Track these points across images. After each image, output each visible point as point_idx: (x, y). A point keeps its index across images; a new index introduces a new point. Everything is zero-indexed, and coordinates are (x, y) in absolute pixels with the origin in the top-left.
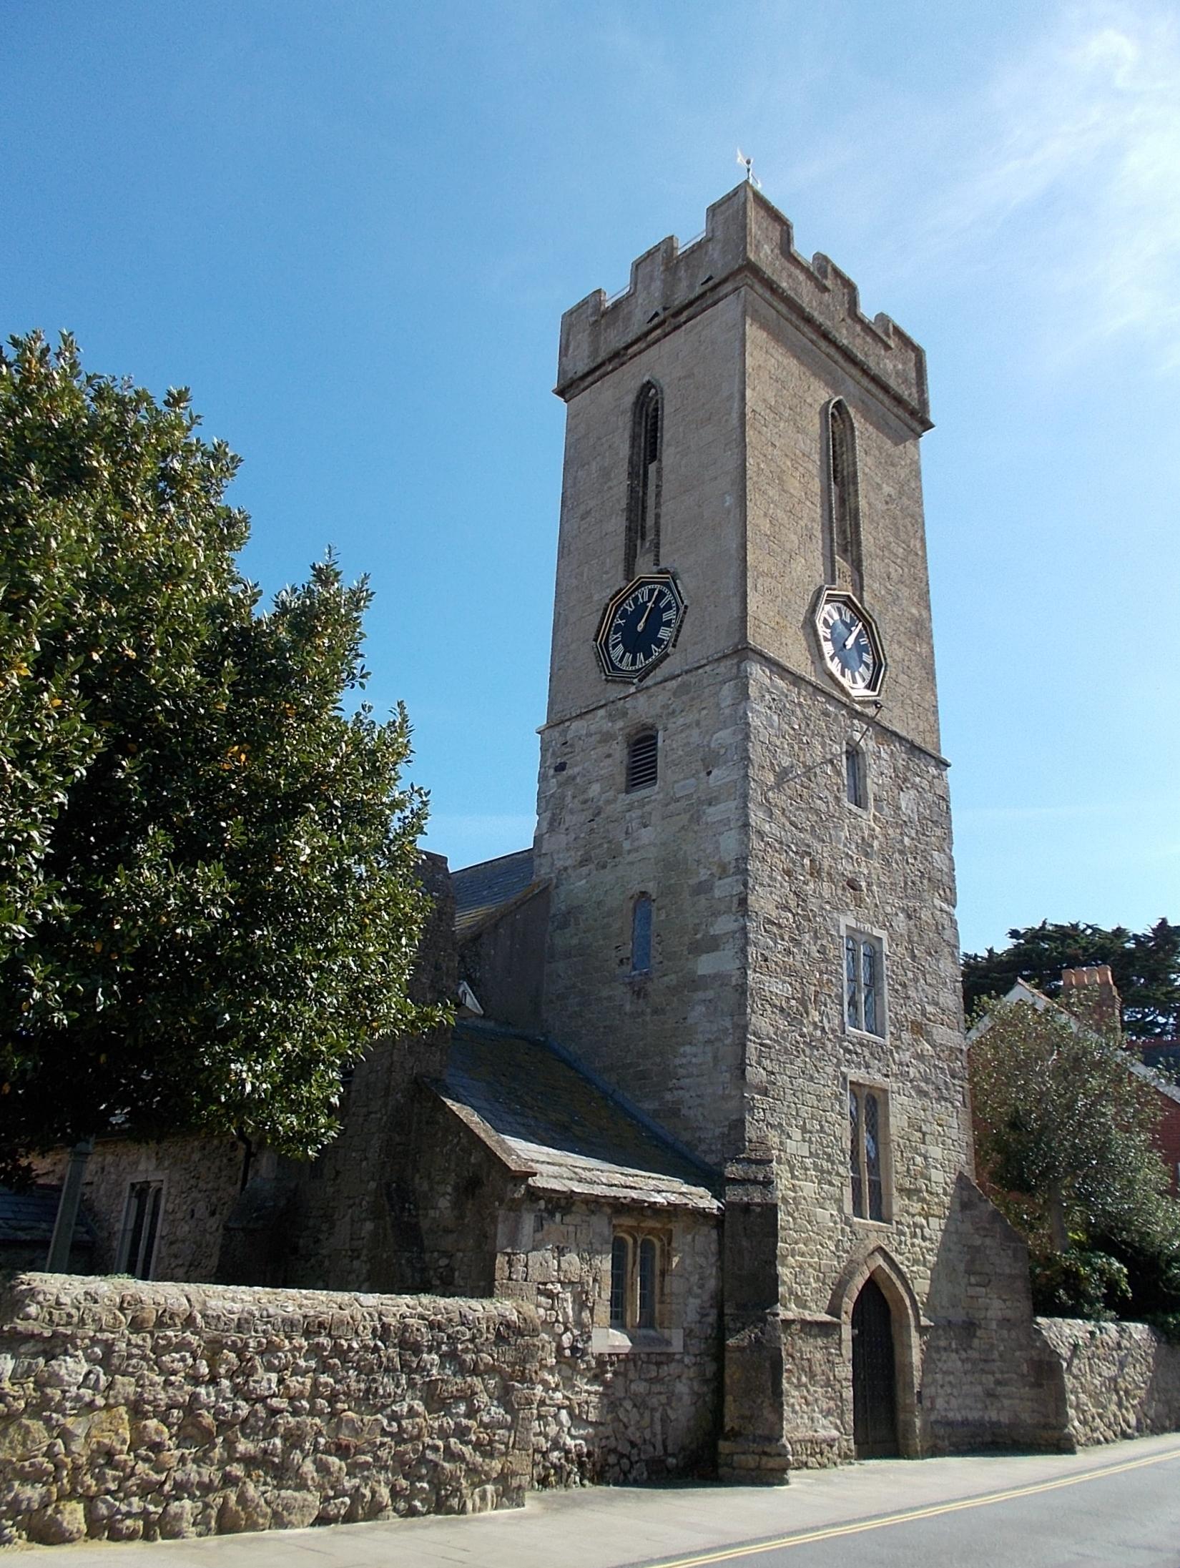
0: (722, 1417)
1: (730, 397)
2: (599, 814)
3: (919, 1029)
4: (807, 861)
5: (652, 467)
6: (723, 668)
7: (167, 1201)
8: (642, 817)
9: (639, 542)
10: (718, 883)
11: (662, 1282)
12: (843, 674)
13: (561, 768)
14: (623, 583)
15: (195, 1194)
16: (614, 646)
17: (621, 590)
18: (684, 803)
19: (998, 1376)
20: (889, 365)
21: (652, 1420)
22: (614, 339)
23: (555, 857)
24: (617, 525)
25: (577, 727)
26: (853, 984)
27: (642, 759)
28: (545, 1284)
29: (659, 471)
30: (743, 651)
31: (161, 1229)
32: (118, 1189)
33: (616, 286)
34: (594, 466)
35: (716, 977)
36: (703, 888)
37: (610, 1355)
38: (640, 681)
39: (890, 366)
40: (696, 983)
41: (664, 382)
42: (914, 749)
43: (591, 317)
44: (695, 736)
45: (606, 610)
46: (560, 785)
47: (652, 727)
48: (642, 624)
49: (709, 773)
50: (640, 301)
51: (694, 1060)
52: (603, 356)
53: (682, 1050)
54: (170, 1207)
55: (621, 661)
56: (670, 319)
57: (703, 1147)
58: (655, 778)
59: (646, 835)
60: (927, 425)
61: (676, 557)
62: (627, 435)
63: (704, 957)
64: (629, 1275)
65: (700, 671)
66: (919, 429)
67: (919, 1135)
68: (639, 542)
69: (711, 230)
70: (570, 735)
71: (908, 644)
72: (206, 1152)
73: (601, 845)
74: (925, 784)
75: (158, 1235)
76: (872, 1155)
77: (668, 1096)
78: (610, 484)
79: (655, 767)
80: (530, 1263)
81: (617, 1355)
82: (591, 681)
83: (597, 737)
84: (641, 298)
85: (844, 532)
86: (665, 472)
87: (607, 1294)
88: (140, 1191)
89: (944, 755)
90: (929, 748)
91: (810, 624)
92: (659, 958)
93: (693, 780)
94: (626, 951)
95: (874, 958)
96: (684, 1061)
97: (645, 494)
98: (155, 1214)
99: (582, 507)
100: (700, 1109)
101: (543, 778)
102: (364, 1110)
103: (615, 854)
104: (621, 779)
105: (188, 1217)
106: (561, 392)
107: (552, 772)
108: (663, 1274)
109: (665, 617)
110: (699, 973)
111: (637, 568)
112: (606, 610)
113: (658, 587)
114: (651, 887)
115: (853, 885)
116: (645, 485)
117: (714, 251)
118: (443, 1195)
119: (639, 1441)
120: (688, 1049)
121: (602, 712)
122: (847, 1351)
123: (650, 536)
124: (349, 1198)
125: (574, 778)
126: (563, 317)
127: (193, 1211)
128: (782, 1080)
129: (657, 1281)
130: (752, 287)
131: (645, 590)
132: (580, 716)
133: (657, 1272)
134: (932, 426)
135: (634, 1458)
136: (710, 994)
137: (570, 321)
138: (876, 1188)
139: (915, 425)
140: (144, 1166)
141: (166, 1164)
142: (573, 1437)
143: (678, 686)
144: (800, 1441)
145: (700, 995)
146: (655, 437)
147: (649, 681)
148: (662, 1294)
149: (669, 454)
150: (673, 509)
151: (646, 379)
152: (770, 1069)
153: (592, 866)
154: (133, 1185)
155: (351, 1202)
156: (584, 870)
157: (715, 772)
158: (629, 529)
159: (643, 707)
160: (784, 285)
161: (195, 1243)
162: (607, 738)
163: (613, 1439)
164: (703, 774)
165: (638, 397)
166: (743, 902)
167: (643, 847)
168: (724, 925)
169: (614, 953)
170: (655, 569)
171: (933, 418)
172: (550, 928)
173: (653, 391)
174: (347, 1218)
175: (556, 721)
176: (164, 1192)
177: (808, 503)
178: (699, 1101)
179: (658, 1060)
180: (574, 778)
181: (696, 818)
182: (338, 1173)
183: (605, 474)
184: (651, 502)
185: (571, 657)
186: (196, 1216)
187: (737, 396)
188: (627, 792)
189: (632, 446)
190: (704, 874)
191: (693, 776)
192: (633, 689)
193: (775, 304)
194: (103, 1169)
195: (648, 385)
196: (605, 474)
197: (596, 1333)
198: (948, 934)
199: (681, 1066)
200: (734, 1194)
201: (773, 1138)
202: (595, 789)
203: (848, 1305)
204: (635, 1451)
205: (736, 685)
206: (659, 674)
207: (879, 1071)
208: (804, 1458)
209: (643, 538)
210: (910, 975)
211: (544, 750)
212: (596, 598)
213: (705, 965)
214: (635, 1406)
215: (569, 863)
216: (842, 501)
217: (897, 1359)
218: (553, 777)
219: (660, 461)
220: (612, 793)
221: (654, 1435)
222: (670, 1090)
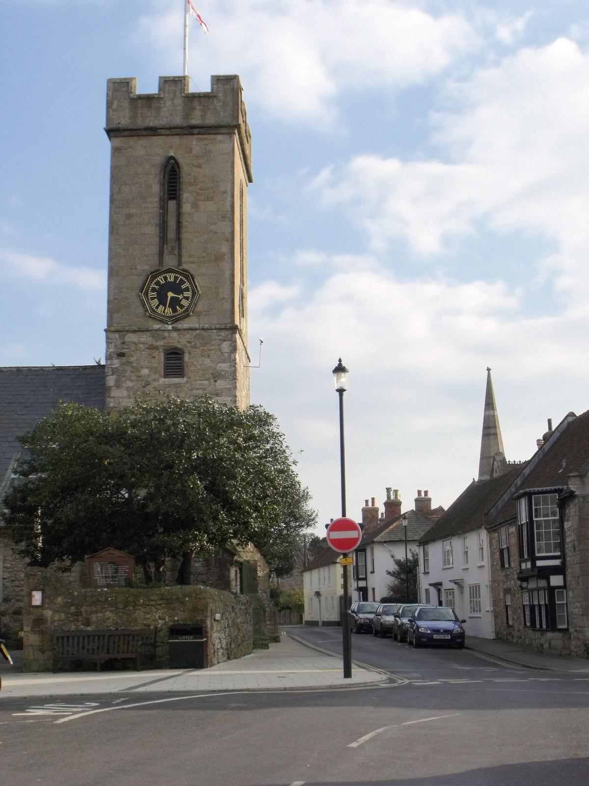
2: (148, 384)
17: (158, 271)
25: (131, 338)
49: (216, 381)
68: (165, 246)
109: (183, 287)
131: (173, 275)
132: (134, 332)
147: (179, 325)
157: (219, 382)
159: (175, 340)
162: (153, 348)
164: (212, 381)
168: (224, 366)
187: (229, 194)
188: (165, 378)
192: (170, 327)
202: (145, 371)
205: (230, 344)
218: (116, 359)
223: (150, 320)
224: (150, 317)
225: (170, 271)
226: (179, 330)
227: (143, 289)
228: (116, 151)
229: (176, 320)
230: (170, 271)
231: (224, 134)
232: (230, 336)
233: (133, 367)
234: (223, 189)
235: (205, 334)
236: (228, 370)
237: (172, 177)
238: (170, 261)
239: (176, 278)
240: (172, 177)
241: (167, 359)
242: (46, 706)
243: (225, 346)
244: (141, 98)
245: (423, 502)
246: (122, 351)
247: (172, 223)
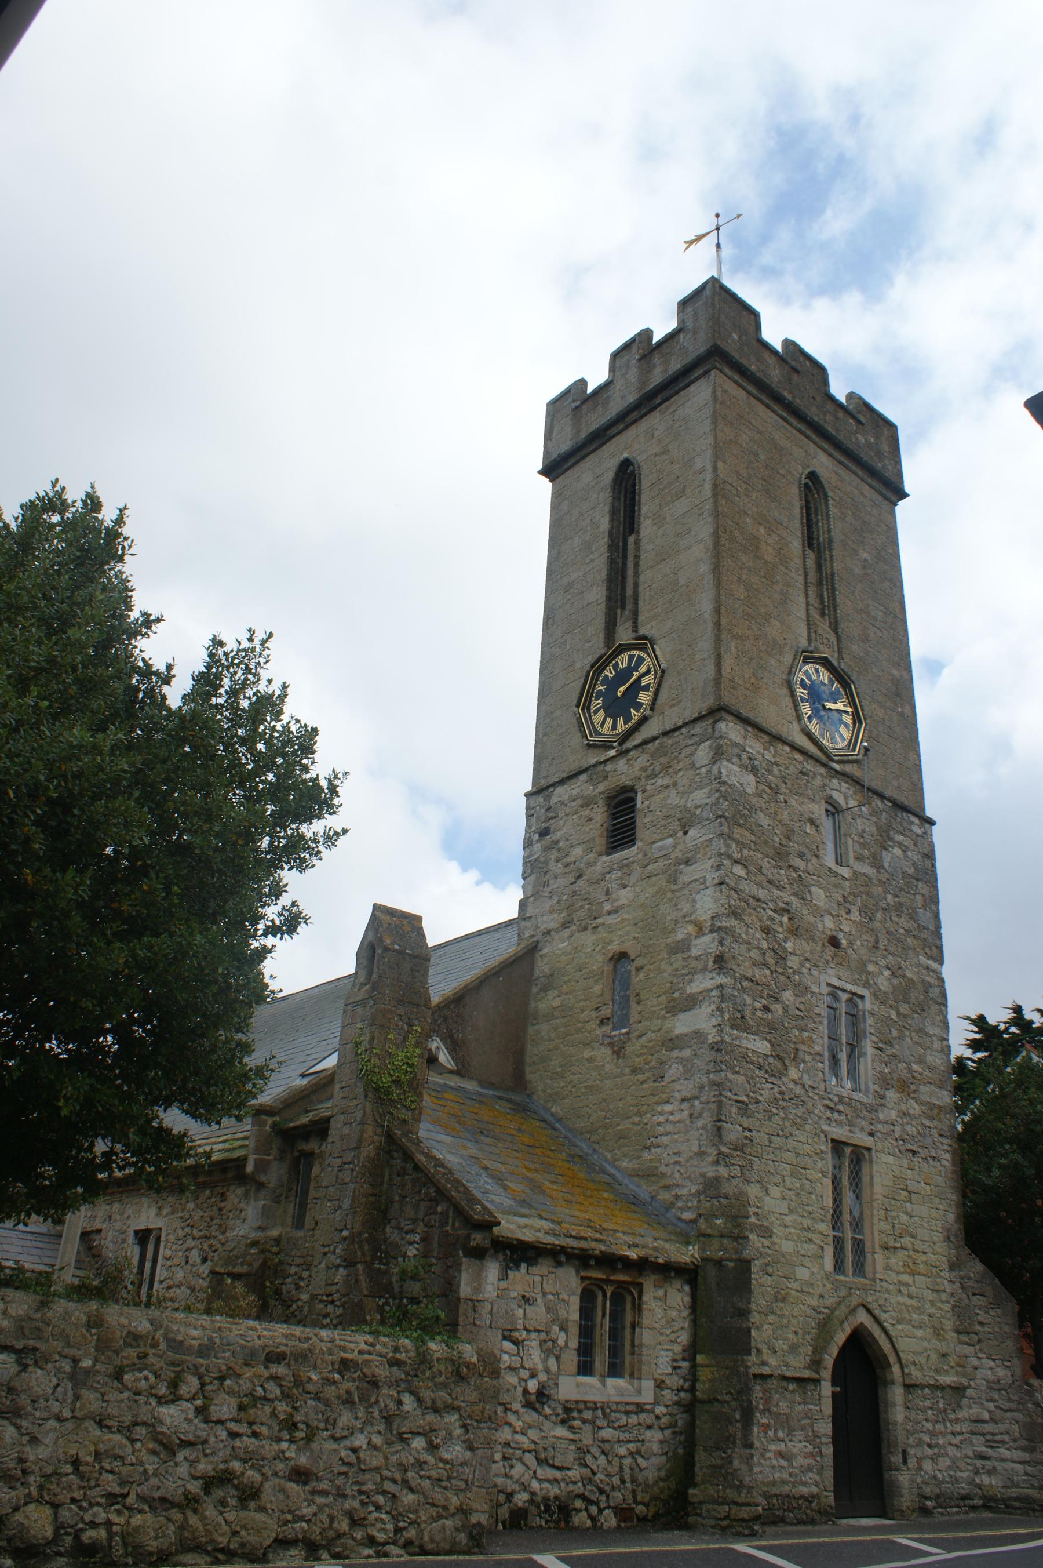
0: (693, 1465)
1: (703, 470)
2: (580, 876)
3: (904, 1087)
4: (785, 919)
5: (631, 539)
6: (698, 729)
7: (165, 1247)
8: (621, 878)
9: (619, 611)
10: (694, 943)
11: (633, 1333)
12: (822, 735)
14: (603, 651)
15: (190, 1243)
16: (596, 712)
17: (601, 657)
18: (660, 864)
19: (988, 1437)
20: (861, 440)
21: (621, 1468)
22: (595, 420)
23: (540, 919)
24: (597, 594)
25: (561, 793)
26: (833, 1043)
28: (511, 1330)
29: (637, 543)
31: (160, 1273)
32: (123, 1236)
33: (597, 376)
34: (577, 541)
36: (683, 947)
37: (577, 1402)
38: (620, 744)
39: (861, 439)
40: (673, 1043)
41: (640, 458)
42: (899, 807)
43: (571, 404)
44: (673, 799)
45: (587, 677)
46: (547, 849)
47: (632, 789)
48: (622, 689)
49: (686, 833)
50: (618, 387)
51: (671, 1118)
52: (583, 435)
53: (659, 1109)
54: (168, 1253)
55: (602, 726)
56: (651, 400)
57: (680, 1204)
58: (634, 840)
59: (624, 896)
60: (905, 495)
61: (653, 623)
62: (607, 508)
63: (681, 1016)
64: (598, 1326)
65: (677, 733)
66: (893, 498)
67: (905, 1193)
68: (619, 611)
69: (681, 321)
70: (554, 799)
71: (888, 704)
72: (199, 1202)
73: (582, 907)
74: (908, 842)
75: (157, 1278)
76: (856, 1214)
77: (646, 1155)
78: (591, 556)
79: (634, 828)
80: (495, 1310)
81: (585, 1402)
83: (579, 802)
84: (618, 385)
85: (821, 596)
86: (643, 542)
87: (574, 1344)
88: (143, 1237)
89: (929, 813)
90: (913, 806)
91: (790, 686)
92: (637, 1017)
93: (670, 841)
94: (606, 1012)
95: (855, 1018)
96: (662, 1119)
97: (624, 564)
98: (155, 1261)
99: (565, 580)
100: (678, 1168)
101: (528, 844)
102: (339, 1161)
104: (601, 843)
105: (183, 1264)
106: (546, 472)
107: (536, 837)
108: (633, 1327)
110: (678, 1031)
111: (617, 636)
112: (587, 677)
113: (637, 653)
115: (834, 942)
116: (625, 557)
118: (411, 1243)
119: (607, 1488)
120: (668, 1108)
121: (583, 777)
122: (827, 1408)
123: (629, 606)
124: (324, 1246)
125: (557, 842)
126: (548, 405)
127: (187, 1257)
128: (760, 1137)
129: (628, 1331)
130: (721, 371)
131: (625, 656)
132: (562, 782)
133: (628, 1324)
134: (906, 495)
135: (603, 1505)
136: (687, 1053)
137: (555, 407)
138: (859, 1246)
139: (889, 494)
140: (146, 1214)
141: (165, 1212)
142: (540, 1481)
143: (657, 749)
144: (776, 1495)
145: (676, 1053)
146: (633, 511)
147: (629, 744)
148: (633, 1345)
149: (647, 528)
151: (625, 455)
152: (746, 1125)
153: (574, 928)
154: (136, 1232)
155: (326, 1249)
156: (567, 933)
158: (609, 599)
159: (623, 772)
160: (753, 368)
161: (189, 1288)
162: (588, 803)
163: (580, 1484)
164: (680, 834)
165: (617, 474)
167: (622, 907)
169: (594, 1014)
170: (634, 635)
171: (907, 488)
172: (534, 990)
173: (631, 468)
174: (323, 1265)
175: (539, 791)
176: (163, 1238)
177: (783, 569)
178: (677, 1159)
179: (637, 1119)
180: (557, 842)
182: (316, 1223)
184: (630, 572)
185: (555, 723)
186: (191, 1262)
188: (608, 854)
189: (612, 521)
191: (671, 836)
192: (612, 753)
193: (745, 385)
194: (110, 1217)
195: (626, 463)
197: (563, 1380)
198: (934, 992)
199: (659, 1124)
201: (753, 1191)
202: (578, 851)
203: (829, 1361)
204: (603, 1498)
206: (638, 738)
207: (862, 1129)
208: (780, 1513)
209: (623, 607)
210: (895, 1033)
211: (529, 816)
212: (578, 665)
214: (603, 1452)
215: (552, 925)
216: (819, 567)
217: (882, 1416)
218: (538, 841)
219: (638, 532)
220: (592, 855)
221: (623, 1481)
222: (648, 1148)
223: (591, 751)
224: (589, 745)
226: (628, 751)
227: (584, 703)
230: (621, 649)
231: (697, 379)
232: (710, 730)
233: (559, 850)
234: (698, 466)
235: (668, 741)
236: (708, 801)
237: (626, 482)
239: (631, 658)
240: (626, 482)
241: (614, 816)
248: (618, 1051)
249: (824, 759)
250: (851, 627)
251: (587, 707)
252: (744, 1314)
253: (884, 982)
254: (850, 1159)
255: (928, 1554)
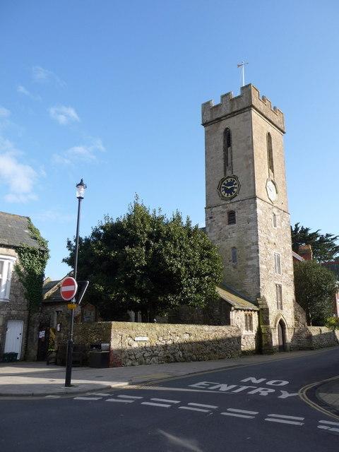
1: (249, 137)
3: (286, 272)
13: (211, 218)
24: (221, 162)
25: (214, 209)
27: (232, 217)
30: (256, 197)
33: (215, 102)
35: (253, 265)
40: (248, 266)
41: (231, 129)
46: (212, 222)
52: (214, 118)
59: (234, 235)
82: (217, 200)
101: (207, 220)
103: (226, 238)
114: (236, 246)
117: (243, 99)
147: (233, 201)
150: (237, 161)
159: (232, 207)
162: (223, 212)
166: (258, 251)
181: (246, 232)
183: (217, 148)
190: (248, 245)
196: (217, 148)
200: (261, 307)
201: (265, 295)
202: (220, 223)
213: (250, 263)
225: (228, 177)
227: (219, 188)
228: (207, 133)
229: (231, 199)
230: (228, 177)
237: (228, 135)
238: (229, 173)
240: (228, 135)
241: (229, 216)
242: (280, 327)
243: (252, 206)
244: (215, 107)
245: (189, 223)
246: (231, 226)
247: (229, 157)
248: (235, 267)
249: (270, 202)
250: (276, 176)
251: (220, 190)
252: (268, 318)
253: (283, 251)
254: (279, 288)
255: (216, 385)
